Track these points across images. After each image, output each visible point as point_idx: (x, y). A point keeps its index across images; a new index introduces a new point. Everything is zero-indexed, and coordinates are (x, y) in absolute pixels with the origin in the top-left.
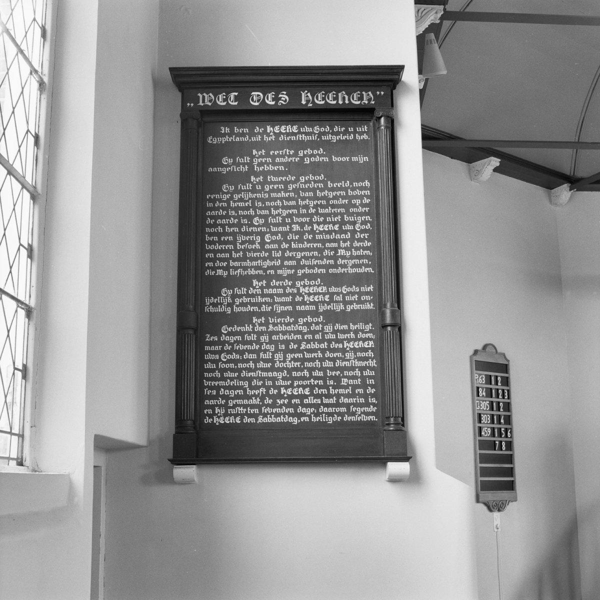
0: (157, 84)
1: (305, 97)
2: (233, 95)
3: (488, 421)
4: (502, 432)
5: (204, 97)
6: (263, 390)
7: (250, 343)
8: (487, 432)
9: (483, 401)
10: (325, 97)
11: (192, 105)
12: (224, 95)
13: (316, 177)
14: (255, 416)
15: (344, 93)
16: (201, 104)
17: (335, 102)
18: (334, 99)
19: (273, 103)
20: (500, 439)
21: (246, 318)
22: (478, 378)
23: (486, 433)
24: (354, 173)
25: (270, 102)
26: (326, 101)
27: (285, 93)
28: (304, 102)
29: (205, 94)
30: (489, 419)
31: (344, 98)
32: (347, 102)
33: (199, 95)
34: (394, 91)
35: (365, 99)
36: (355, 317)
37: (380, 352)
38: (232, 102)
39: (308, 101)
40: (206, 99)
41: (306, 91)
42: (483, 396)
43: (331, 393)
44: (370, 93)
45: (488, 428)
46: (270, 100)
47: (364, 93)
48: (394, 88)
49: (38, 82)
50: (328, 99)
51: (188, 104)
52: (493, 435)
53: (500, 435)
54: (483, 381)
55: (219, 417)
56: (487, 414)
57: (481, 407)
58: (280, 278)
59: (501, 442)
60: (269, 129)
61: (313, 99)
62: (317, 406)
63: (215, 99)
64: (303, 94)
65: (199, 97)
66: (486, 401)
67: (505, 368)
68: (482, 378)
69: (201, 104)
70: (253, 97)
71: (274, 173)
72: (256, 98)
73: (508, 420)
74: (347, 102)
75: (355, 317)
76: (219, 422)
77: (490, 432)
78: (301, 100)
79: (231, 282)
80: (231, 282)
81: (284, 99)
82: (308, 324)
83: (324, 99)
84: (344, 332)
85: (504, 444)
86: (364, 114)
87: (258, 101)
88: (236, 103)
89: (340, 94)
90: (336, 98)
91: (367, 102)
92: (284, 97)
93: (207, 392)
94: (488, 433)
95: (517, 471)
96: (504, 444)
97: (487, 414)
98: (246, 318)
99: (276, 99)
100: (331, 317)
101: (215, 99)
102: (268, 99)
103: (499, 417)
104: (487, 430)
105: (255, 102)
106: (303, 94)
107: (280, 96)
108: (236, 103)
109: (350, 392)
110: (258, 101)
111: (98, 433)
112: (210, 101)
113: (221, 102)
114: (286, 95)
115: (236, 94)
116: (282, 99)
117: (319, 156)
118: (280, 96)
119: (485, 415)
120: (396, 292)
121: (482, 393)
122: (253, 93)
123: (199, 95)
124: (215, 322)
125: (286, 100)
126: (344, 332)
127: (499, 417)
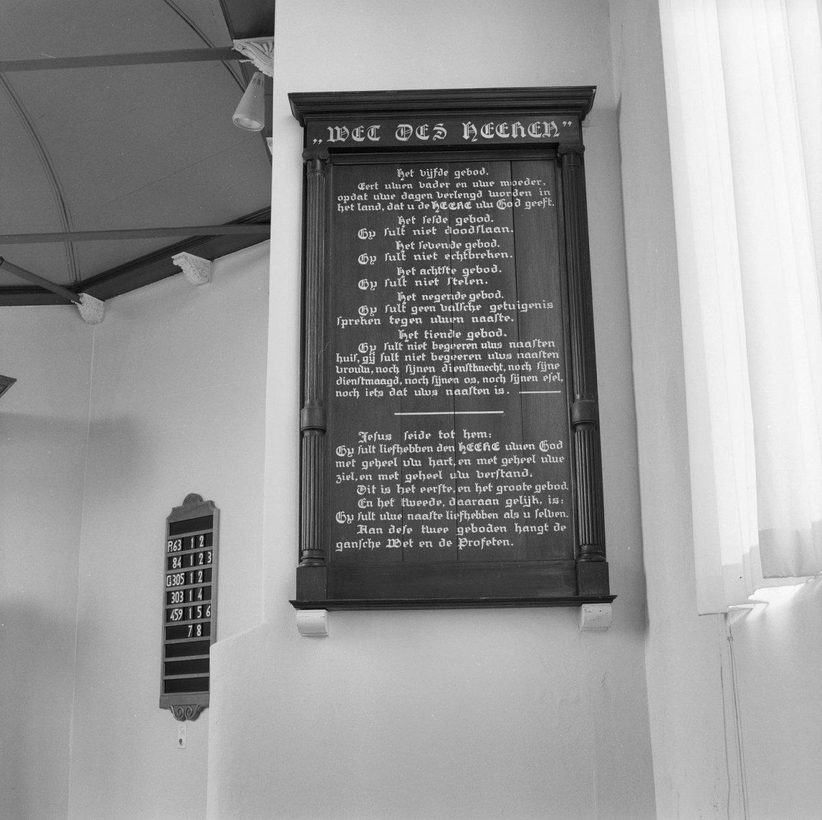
2: (374, 128)
3: (180, 599)
4: (198, 611)
5: (335, 132)
6: (396, 446)
8: (177, 613)
9: (176, 574)
10: (495, 129)
11: (320, 141)
12: (361, 129)
13: (478, 219)
15: (519, 123)
16: (332, 139)
17: (507, 136)
18: (506, 132)
19: (426, 138)
20: (195, 621)
22: (173, 546)
23: (175, 617)
25: (423, 137)
26: (496, 135)
27: (442, 125)
29: (337, 128)
30: (182, 597)
31: (519, 131)
32: (523, 135)
33: (330, 128)
34: (584, 123)
35: (546, 131)
38: (373, 137)
39: (472, 135)
40: (337, 134)
41: (470, 123)
42: (178, 567)
43: (465, 437)
44: (553, 123)
45: (179, 608)
46: (422, 133)
47: (545, 123)
48: (583, 118)
50: (499, 131)
51: (315, 141)
52: (185, 617)
54: (178, 547)
55: (465, 444)
56: (179, 591)
57: (173, 582)
59: (195, 626)
63: (350, 134)
64: (465, 126)
65: (329, 131)
66: (180, 573)
68: (177, 545)
69: (332, 139)
70: (399, 131)
72: (404, 133)
73: (207, 593)
74: (523, 135)
76: (467, 451)
77: (181, 614)
78: (463, 134)
81: (440, 133)
83: (492, 132)
85: (199, 628)
86: (548, 149)
87: (407, 136)
88: (377, 139)
89: (513, 126)
90: (509, 131)
91: (549, 135)
92: (440, 129)
93: (407, 437)
94: (179, 616)
96: (199, 628)
97: (179, 591)
99: (431, 132)
101: (350, 134)
102: (419, 133)
103: (195, 591)
104: (177, 612)
105: (403, 137)
106: (465, 126)
107: (436, 128)
108: (377, 139)
109: (396, 465)
110: (407, 136)
113: (488, 134)
114: (443, 127)
116: (439, 132)
118: (436, 128)
119: (177, 593)
120: (306, 383)
121: (176, 563)
122: (400, 126)
123: (330, 128)
125: (443, 133)
127: (195, 591)
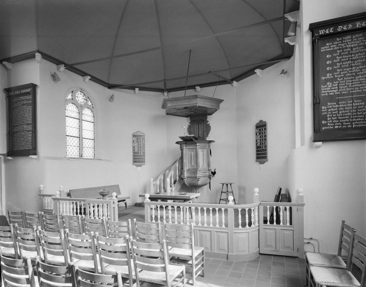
2: (331, 29)
7: (18, 136)
14: (19, 148)
16: (320, 34)
28: (357, 26)
39: (359, 26)
52: (260, 144)
53: (263, 144)
58: (21, 125)
59: (263, 146)
60: (338, 39)
61: (361, 24)
62: (26, 146)
69: (320, 34)
71: (345, 55)
72: (340, 28)
82: (25, 132)
84: (29, 133)
95: (146, 155)
99: (347, 27)
112: (323, 32)
115: (333, 28)
121: (258, 134)
124: (14, 133)
126: (29, 133)
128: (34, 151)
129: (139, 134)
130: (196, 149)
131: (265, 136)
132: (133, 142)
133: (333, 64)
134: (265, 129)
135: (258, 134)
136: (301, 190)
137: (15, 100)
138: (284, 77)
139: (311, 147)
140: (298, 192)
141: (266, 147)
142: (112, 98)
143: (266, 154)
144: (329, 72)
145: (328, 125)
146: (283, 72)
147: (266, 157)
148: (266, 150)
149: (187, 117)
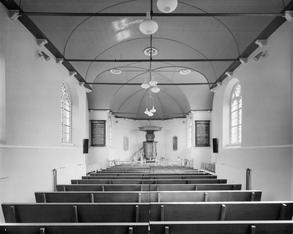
0: (89, 121)
1: (99, 122)
8: (125, 144)
21: (95, 137)
24: (102, 127)
36: (102, 137)
37: (104, 139)
49: (144, 21)
67: (177, 138)
75: (102, 137)
79: (95, 135)
80: (95, 135)
98: (95, 137)
100: (101, 137)
111: (213, 152)
117: (100, 126)
121: (174, 140)
128: (104, 145)
129: (126, 137)
130: (153, 145)
131: (177, 141)
132: (124, 140)
133: (199, 130)
134: (177, 139)
135: (174, 140)
136: (193, 158)
137: (94, 125)
138: (184, 124)
139: (195, 148)
140: (192, 158)
141: (177, 145)
142: (117, 122)
143: (177, 147)
144: (199, 131)
145: (198, 143)
146: (184, 122)
147: (177, 149)
148: (177, 146)
149: (145, 131)
